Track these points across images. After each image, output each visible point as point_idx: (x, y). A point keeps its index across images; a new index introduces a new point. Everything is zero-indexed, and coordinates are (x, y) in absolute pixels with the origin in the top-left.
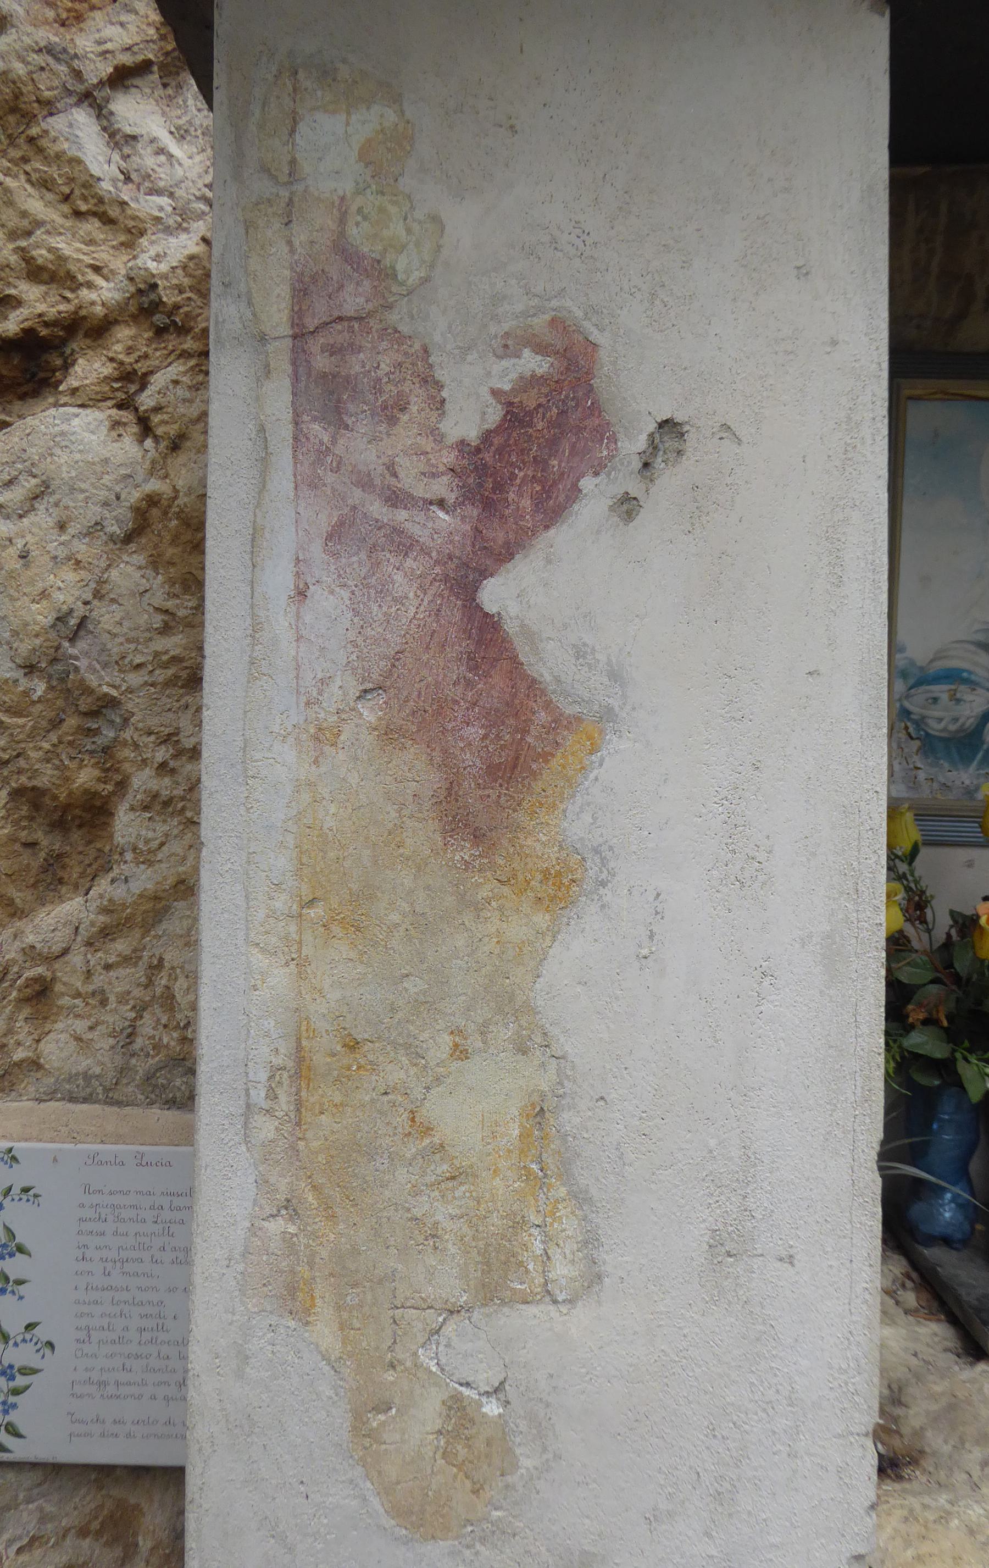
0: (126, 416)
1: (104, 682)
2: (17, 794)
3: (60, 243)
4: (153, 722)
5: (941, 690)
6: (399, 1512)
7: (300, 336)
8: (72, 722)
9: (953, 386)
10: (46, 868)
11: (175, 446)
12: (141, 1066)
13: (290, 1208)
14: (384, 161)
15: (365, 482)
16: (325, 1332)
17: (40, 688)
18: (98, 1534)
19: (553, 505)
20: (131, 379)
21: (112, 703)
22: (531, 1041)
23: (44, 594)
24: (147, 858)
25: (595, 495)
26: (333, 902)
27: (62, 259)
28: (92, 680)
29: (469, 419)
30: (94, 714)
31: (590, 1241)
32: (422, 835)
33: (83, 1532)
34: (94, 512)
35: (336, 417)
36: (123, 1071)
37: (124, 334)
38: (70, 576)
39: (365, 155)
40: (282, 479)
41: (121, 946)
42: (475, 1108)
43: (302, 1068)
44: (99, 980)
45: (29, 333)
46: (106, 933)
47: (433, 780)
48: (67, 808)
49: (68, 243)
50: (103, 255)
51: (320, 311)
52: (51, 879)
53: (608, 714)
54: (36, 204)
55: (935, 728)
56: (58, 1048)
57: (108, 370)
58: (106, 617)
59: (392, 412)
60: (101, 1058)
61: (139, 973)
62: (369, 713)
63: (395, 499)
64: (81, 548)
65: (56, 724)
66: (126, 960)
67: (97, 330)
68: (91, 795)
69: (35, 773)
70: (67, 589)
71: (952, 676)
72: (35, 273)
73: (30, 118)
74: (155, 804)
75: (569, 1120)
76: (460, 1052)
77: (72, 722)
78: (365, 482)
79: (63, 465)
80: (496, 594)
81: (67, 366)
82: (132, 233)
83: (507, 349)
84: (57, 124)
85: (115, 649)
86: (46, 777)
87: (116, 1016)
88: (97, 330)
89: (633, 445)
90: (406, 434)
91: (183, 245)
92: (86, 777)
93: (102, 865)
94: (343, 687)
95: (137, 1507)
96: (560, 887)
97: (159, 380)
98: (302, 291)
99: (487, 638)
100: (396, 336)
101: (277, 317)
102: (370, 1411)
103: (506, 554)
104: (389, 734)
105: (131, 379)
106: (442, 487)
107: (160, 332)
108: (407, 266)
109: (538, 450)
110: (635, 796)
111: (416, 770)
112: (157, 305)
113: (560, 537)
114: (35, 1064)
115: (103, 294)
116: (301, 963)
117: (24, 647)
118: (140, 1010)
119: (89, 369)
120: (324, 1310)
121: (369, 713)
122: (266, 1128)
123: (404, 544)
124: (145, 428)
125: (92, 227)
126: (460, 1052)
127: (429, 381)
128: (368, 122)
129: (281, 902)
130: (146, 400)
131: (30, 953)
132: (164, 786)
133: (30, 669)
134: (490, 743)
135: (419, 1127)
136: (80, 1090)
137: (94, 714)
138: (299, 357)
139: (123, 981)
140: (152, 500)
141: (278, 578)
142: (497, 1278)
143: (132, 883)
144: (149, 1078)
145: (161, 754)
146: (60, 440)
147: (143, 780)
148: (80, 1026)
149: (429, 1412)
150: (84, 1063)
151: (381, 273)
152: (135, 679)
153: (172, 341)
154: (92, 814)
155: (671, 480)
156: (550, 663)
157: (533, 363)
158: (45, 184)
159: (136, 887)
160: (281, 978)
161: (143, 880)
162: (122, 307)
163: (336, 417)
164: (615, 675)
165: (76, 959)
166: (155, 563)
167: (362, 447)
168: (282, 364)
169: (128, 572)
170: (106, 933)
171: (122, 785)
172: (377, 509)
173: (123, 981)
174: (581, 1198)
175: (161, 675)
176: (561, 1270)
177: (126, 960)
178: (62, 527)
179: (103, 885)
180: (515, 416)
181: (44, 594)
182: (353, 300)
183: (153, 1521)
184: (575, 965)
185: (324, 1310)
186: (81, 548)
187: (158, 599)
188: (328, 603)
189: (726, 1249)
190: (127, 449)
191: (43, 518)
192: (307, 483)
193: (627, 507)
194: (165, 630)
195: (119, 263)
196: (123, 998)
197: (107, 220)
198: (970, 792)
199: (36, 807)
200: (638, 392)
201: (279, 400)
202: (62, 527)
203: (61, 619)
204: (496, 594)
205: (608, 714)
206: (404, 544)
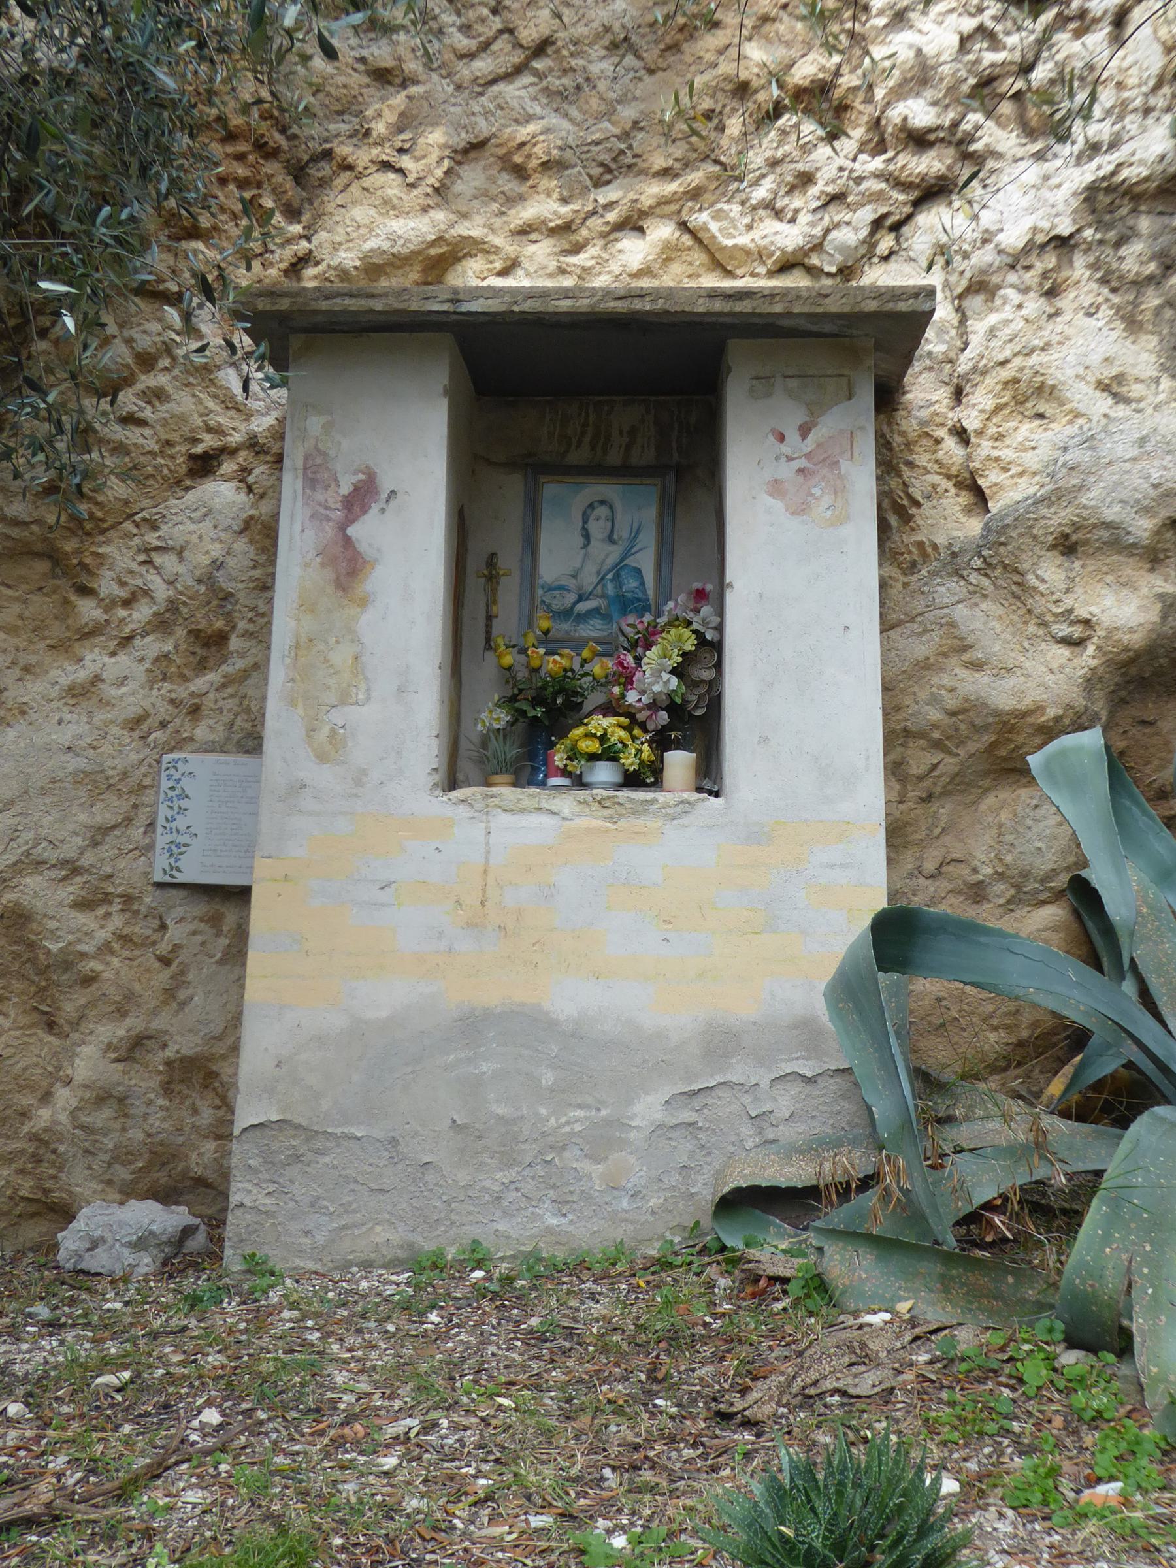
0: (242, 485)
1: (229, 587)
2: (190, 632)
3: (220, 419)
4: (247, 603)
5: (556, 593)
6: (317, 757)
7: (305, 469)
8: (215, 602)
9: (560, 478)
10: (200, 662)
11: (262, 496)
12: (236, 737)
13: (293, 680)
14: (327, 428)
15: (320, 504)
16: (300, 711)
17: (203, 589)
18: (207, 922)
19: (364, 511)
20: (245, 471)
21: (231, 595)
22: (356, 640)
23: (207, 552)
24: (242, 655)
25: (375, 508)
26: (307, 606)
27: (220, 425)
28: (224, 586)
29: (345, 489)
30: (224, 599)
31: (368, 690)
32: (330, 589)
33: (201, 920)
34: (228, 521)
35: (313, 489)
36: (228, 739)
37: (243, 454)
38: (218, 545)
39: (323, 427)
40: (299, 504)
41: (230, 690)
42: (341, 656)
43: (297, 646)
44: (221, 703)
45: (205, 453)
46: (224, 686)
47: (334, 576)
48: (210, 637)
49: (222, 419)
50: (236, 424)
51: (310, 463)
52: (202, 666)
53: (376, 560)
54: (211, 404)
55: (555, 608)
56: (202, 732)
57: (236, 467)
58: (231, 562)
59: (327, 487)
60: (219, 734)
61: (237, 701)
62: (318, 560)
63: (327, 508)
64: (223, 535)
65: (208, 603)
66: (231, 696)
67: (231, 452)
68: (221, 631)
69: (198, 623)
70: (216, 550)
71: (561, 588)
72: (209, 430)
73: (211, 372)
74: (247, 634)
75: (364, 659)
76: (337, 642)
77: (215, 602)
78: (320, 504)
79: (217, 503)
80: (350, 531)
81: (219, 466)
82: (248, 416)
83: (355, 473)
84: (221, 374)
85: (234, 574)
86: (203, 624)
87: (227, 717)
88: (231, 452)
89: (384, 496)
90: (330, 493)
91: (269, 420)
92: (219, 624)
93: (224, 660)
94: (311, 555)
95: (223, 914)
96: (364, 602)
97: (256, 472)
98: (306, 458)
99: (348, 541)
100: (328, 469)
101: (300, 464)
102: (311, 730)
103: (353, 522)
104: (323, 565)
105: (245, 471)
106: (338, 506)
107: (257, 453)
108: (332, 453)
109: (362, 497)
110: (383, 580)
111: (329, 573)
112: (257, 443)
113: (366, 517)
114: (191, 739)
115: (236, 438)
116: (299, 620)
117: (198, 573)
118: (236, 715)
119: (228, 467)
120: (300, 705)
121: (318, 560)
122: (288, 661)
123: (328, 519)
124: (250, 489)
125: (233, 413)
126: (337, 642)
127: (336, 480)
128: (323, 419)
129: (295, 605)
130: (251, 479)
131: (192, 695)
132: (251, 627)
133: (199, 581)
134: (348, 567)
135: (326, 661)
136: (210, 748)
137: (224, 599)
138: (305, 474)
139: (231, 703)
140: (251, 517)
141: (298, 527)
142: (345, 699)
143: (236, 665)
144: (238, 742)
145: (250, 615)
146: (217, 494)
147: (242, 625)
148: (211, 722)
149: (326, 730)
150: (212, 737)
151: (326, 455)
152: (241, 586)
153: (262, 457)
154: (221, 639)
155: (393, 503)
156: (363, 547)
157: (361, 476)
158: (216, 396)
159: (237, 667)
160: (293, 624)
161: (240, 664)
162: (243, 444)
163: (313, 489)
164: (379, 550)
165: (211, 696)
166: (251, 542)
167: (320, 496)
168: (301, 475)
169: (241, 545)
170: (224, 686)
171: (234, 627)
172: (323, 511)
173: (231, 703)
174: (366, 679)
175: (252, 585)
176: (361, 697)
177: (231, 696)
178: (215, 527)
179: (224, 667)
180: (357, 489)
181: (207, 552)
182: (318, 461)
183: (230, 918)
184: (366, 621)
185: (300, 705)
186: (223, 535)
187: (252, 556)
188: (310, 533)
189: (401, 690)
190: (243, 498)
191: (208, 523)
192: (306, 504)
193: (383, 510)
194: (254, 567)
195: (242, 427)
196: (230, 710)
197: (239, 410)
198: (567, 632)
199: (197, 637)
200: (386, 483)
201: (299, 484)
202: (215, 527)
203: (214, 562)
204: (350, 531)
205: (376, 560)
206: (328, 519)
